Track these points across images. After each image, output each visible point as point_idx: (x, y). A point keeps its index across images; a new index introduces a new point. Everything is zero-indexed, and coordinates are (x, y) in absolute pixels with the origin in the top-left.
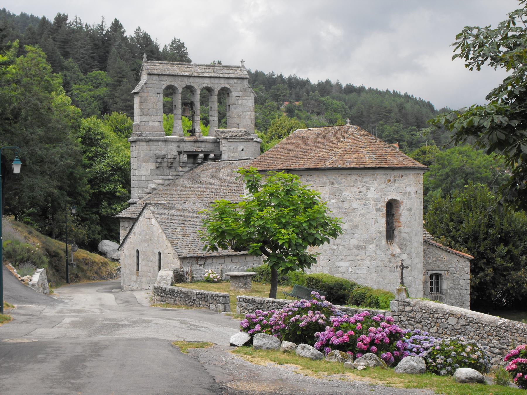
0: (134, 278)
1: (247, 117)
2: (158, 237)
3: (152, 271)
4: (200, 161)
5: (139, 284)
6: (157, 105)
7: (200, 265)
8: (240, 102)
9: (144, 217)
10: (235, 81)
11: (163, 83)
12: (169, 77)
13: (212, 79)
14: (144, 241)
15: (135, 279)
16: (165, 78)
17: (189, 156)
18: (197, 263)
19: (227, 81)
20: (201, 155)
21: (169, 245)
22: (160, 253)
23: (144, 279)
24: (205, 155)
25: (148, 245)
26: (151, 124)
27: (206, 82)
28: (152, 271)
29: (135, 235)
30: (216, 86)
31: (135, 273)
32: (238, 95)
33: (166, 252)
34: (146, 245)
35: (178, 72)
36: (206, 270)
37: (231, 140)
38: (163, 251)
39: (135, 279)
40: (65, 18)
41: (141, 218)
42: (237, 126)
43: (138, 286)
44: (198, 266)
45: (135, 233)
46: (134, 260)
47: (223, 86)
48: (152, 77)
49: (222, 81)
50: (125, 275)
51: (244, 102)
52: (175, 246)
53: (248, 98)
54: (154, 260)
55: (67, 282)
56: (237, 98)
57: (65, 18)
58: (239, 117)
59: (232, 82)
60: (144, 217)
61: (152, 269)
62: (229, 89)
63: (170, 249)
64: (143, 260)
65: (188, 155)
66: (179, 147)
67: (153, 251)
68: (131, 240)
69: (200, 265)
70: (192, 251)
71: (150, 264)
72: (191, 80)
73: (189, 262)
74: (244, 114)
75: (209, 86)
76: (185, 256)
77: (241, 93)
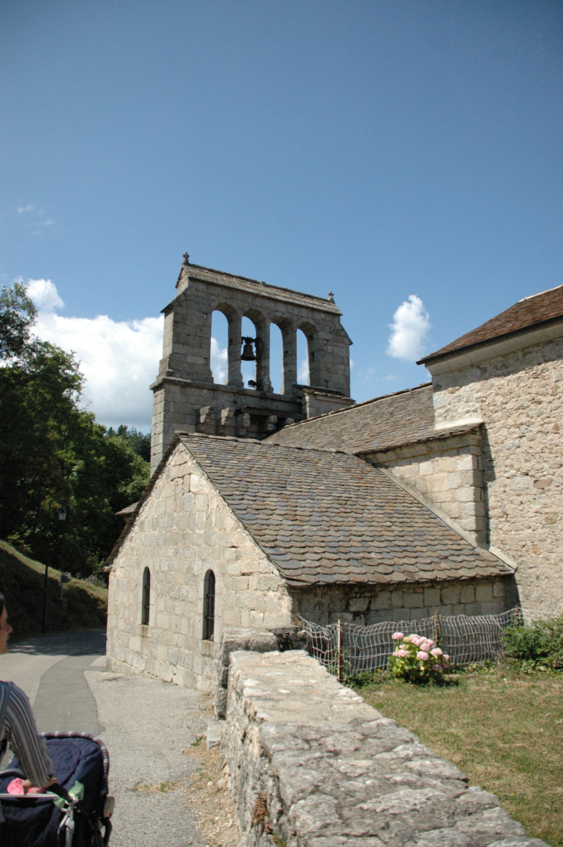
0: (135, 642)
1: (339, 372)
2: (208, 523)
3: (184, 630)
4: (270, 427)
5: (147, 663)
6: (201, 330)
7: (356, 615)
8: (330, 348)
9: (168, 476)
10: (323, 316)
11: (213, 297)
12: (224, 291)
13: (290, 307)
14: (166, 542)
15: (137, 647)
16: (218, 290)
17: (253, 418)
18: (346, 609)
19: (310, 314)
20: (273, 418)
21: (248, 543)
22: (210, 577)
23: (161, 651)
24: (279, 419)
25: (176, 552)
26: (190, 359)
27: (280, 309)
28: (184, 630)
29: (142, 529)
30: (295, 318)
31: (139, 631)
32: (327, 338)
33: (235, 568)
34: (171, 552)
35: (238, 285)
36: (397, 635)
37: (320, 398)
38: (222, 567)
39: (137, 647)
40: (125, 428)
41: (159, 483)
42: (325, 383)
43: (143, 667)
44: (349, 616)
45: (142, 523)
46: (136, 596)
47: (305, 320)
48: (196, 285)
49: (304, 312)
50: (115, 632)
51: (336, 349)
52: (272, 550)
53: (341, 345)
54: (192, 596)
55: (44, 631)
56: (325, 342)
57: (125, 428)
58: (328, 370)
59: (318, 316)
60: (168, 476)
61: (184, 622)
62: (313, 327)
63: (252, 556)
64: (160, 595)
65: (251, 415)
66: (235, 402)
67: (190, 569)
68: (133, 545)
69: (356, 615)
70: (330, 564)
71: (179, 607)
72: (258, 302)
73: (320, 604)
74: (336, 366)
75: (285, 316)
76: (312, 579)
77: (330, 335)
